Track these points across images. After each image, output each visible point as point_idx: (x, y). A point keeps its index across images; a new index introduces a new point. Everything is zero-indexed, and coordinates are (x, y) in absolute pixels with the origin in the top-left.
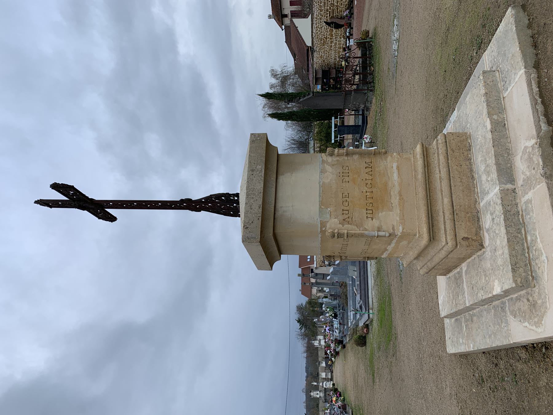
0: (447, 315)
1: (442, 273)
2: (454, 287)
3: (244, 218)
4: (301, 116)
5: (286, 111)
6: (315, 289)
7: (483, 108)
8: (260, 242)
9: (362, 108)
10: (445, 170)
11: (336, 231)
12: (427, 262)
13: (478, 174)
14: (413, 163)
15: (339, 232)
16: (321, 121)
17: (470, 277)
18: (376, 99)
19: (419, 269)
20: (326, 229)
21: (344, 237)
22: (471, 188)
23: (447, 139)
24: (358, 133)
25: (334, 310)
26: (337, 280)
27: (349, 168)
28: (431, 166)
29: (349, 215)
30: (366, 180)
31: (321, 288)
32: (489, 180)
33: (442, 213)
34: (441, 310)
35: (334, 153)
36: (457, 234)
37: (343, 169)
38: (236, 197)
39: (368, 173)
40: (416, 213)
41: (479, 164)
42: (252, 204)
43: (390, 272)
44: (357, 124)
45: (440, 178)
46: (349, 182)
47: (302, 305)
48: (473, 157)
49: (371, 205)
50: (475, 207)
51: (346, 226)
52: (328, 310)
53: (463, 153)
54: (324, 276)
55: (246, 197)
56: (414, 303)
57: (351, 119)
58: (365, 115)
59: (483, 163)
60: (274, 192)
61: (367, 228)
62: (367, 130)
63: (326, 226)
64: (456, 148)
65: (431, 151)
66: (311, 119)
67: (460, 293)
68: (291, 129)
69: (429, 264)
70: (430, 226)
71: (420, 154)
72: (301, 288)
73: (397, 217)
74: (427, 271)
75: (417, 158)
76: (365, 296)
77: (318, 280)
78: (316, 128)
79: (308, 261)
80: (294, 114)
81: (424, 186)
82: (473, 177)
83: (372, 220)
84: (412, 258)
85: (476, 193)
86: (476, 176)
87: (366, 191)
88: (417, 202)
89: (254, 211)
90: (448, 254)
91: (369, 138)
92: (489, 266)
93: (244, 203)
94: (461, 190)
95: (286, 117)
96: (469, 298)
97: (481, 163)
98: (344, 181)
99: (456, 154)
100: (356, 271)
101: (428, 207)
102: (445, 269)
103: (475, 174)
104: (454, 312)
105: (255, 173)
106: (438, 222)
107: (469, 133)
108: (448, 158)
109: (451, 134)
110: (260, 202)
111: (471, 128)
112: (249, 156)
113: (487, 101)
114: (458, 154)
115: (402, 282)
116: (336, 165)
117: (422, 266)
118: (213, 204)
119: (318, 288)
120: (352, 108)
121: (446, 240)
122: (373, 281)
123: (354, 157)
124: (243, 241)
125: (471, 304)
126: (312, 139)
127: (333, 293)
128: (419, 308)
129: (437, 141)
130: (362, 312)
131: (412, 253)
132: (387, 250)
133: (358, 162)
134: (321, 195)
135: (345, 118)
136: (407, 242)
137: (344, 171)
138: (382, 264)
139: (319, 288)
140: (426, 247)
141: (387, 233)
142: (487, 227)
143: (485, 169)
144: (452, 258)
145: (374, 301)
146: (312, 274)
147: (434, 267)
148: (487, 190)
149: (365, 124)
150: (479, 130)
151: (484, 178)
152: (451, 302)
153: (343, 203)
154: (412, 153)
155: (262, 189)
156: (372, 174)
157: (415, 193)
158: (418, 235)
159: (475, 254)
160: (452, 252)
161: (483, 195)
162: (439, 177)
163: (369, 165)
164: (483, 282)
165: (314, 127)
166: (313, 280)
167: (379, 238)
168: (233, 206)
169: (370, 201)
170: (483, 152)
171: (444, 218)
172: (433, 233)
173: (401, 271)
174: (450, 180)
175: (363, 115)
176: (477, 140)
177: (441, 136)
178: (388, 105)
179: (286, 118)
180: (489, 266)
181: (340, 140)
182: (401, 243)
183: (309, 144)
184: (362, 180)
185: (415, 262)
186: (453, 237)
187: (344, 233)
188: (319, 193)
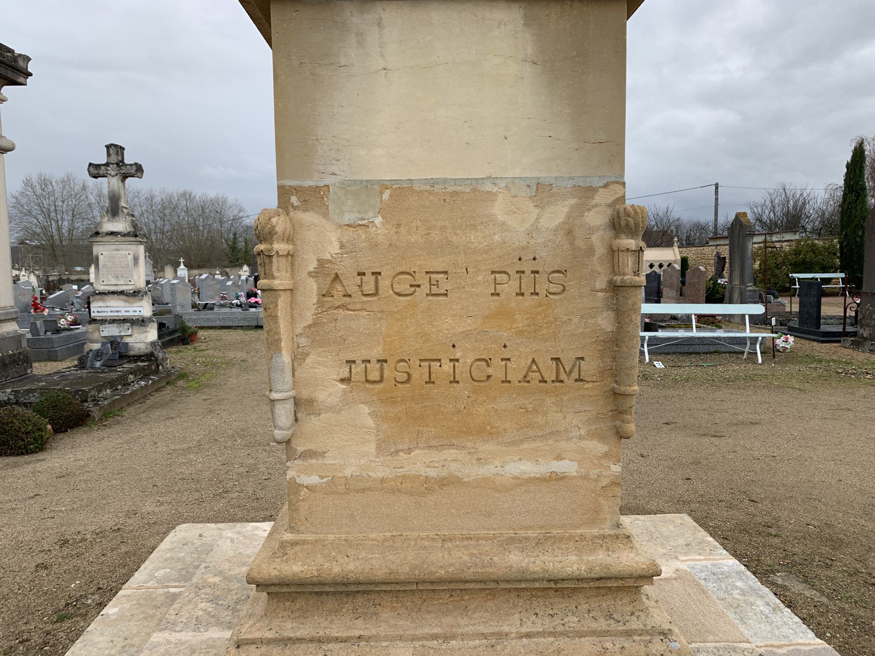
9: (862, 331)
11: (279, 247)
16: (839, 251)
20: (295, 208)
24: (801, 323)
27: (555, 297)
28: (557, 600)
29: (357, 297)
30: (502, 360)
33: (357, 633)
35: (623, 236)
37: (554, 272)
39: (534, 367)
44: (822, 321)
46: (520, 297)
58: (842, 339)
61: (308, 361)
62: (807, 342)
63: (307, 210)
66: (846, 232)
71: (607, 567)
73: (354, 468)
75: (592, 551)
80: (859, 196)
83: (342, 381)
87: (457, 360)
91: (786, 346)
95: (852, 179)
98: (497, 275)
101: (384, 583)
106: (330, 611)
120: (861, 312)
123: (605, 314)
133: (580, 331)
134: (437, 188)
137: (542, 278)
149: (822, 339)
156: (528, 382)
162: (506, 629)
163: (571, 372)
169: (419, 374)
175: (845, 334)
178: (862, 392)
183: (792, 233)
184: (505, 346)
188: (445, 181)
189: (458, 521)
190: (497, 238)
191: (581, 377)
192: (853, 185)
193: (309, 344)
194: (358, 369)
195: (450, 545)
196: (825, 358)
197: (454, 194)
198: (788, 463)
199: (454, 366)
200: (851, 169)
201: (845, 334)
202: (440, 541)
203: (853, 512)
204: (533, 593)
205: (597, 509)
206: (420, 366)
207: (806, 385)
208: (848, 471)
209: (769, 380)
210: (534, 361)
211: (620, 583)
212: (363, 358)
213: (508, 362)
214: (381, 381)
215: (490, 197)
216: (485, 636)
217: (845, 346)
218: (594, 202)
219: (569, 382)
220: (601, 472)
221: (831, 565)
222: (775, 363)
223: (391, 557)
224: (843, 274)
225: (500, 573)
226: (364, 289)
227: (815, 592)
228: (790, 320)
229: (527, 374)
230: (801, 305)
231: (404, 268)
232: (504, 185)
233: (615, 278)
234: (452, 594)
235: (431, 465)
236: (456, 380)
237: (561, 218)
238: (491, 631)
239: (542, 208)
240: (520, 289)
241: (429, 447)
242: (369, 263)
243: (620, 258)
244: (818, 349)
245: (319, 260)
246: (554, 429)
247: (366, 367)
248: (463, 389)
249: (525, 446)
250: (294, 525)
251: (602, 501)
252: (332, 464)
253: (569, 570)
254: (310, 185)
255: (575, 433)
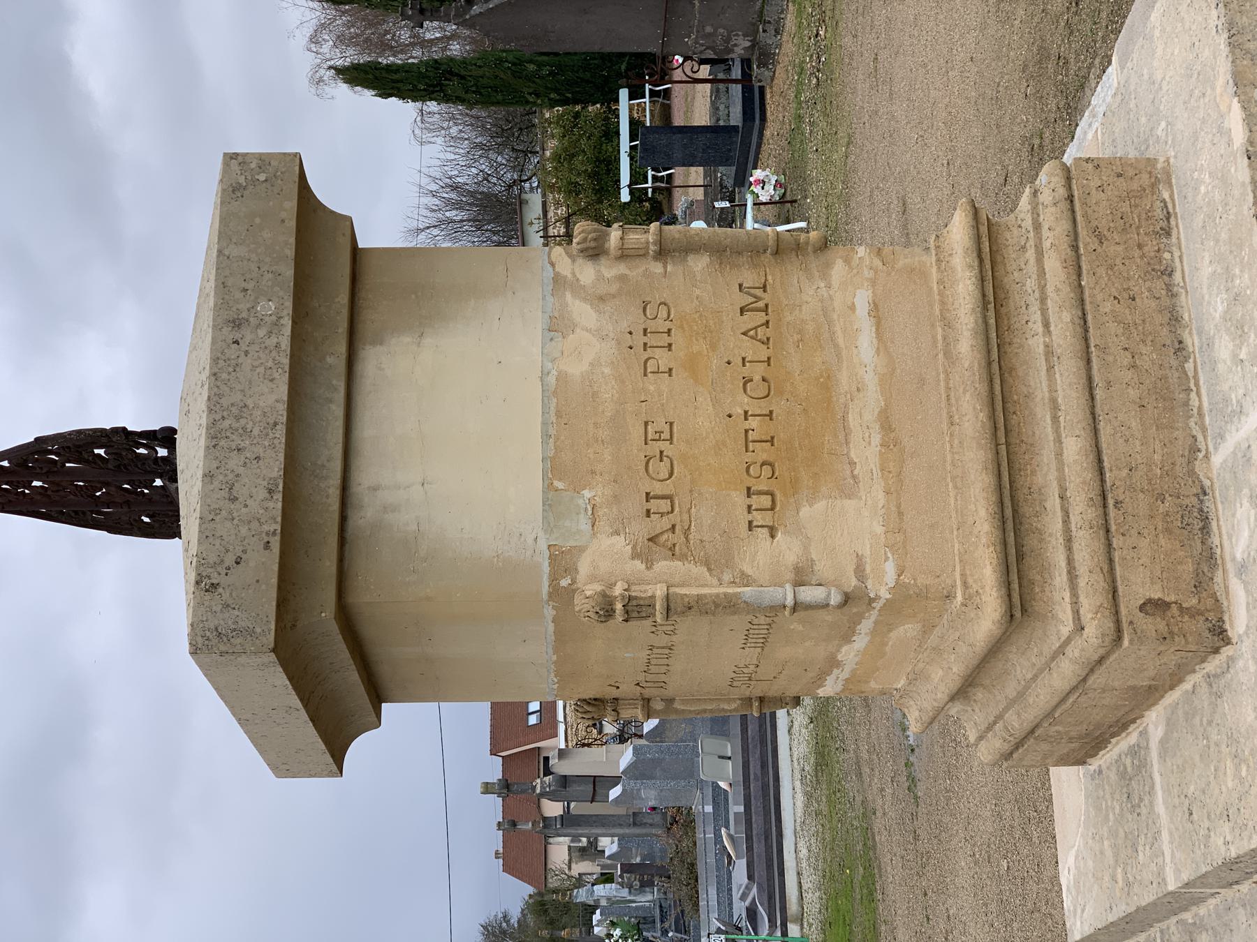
0: (1092, 930)
1: (1068, 754)
2: (1117, 811)
3: (200, 542)
4: (485, 81)
5: (416, 56)
6: (559, 844)
7: (1215, 58)
8: (274, 650)
9: (739, 51)
10: (1067, 317)
11: (618, 590)
12: (1006, 709)
13: (1200, 334)
14: (936, 292)
15: (633, 594)
16: (570, 107)
17: (1178, 766)
18: (800, 12)
19: (972, 739)
20: (574, 581)
21: (654, 616)
22: (1173, 393)
23: (1074, 187)
24: (726, 162)
25: (640, 932)
26: (652, 803)
30: (744, 365)
31: (588, 838)
32: (1241, 357)
33: (1058, 501)
34: (1069, 910)
35: (607, 245)
36: (1121, 589)
37: (645, 315)
38: (161, 446)
39: (752, 333)
40: (952, 502)
41: (1205, 291)
42: (238, 476)
43: (865, 756)
44: (721, 123)
45: (1049, 352)
47: (505, 917)
48: (1181, 262)
49: (767, 471)
50: (1192, 473)
51: (663, 566)
52: (617, 932)
53: (1140, 246)
54: (597, 785)
55: (207, 448)
56: (966, 886)
57: (699, 96)
58: (757, 85)
59: (1218, 288)
60: (340, 423)
62: (764, 148)
64: (1112, 225)
65: (1011, 238)
66: (530, 94)
67: (1143, 837)
68: (440, 140)
69: (1011, 716)
70: (1009, 558)
71: (966, 251)
72: (501, 844)
74: (1007, 747)
76: (769, 866)
77: (573, 805)
78: (553, 136)
79: (530, 723)
80: (451, 73)
81: (982, 388)
82: (1180, 348)
83: (773, 537)
84: (942, 695)
85: (1195, 410)
86: (1193, 341)
87: (746, 412)
88: (957, 457)
89: (244, 510)
90: (1084, 674)
92: (1249, 719)
93: (200, 473)
94: (1134, 402)
96: (1178, 855)
97: (1210, 286)
98: (649, 370)
99: (1112, 248)
100: (730, 758)
101: (999, 476)
102: (1080, 737)
103: (1190, 333)
104: (1120, 919)
105: (247, 335)
106: (1041, 541)
107: (1162, 159)
108: (1080, 267)
109: (1090, 166)
110: (274, 466)
111: (1170, 138)
112: (218, 256)
113: (1231, 25)
114: (1120, 248)
115: (916, 798)
116: (614, 296)
117: (983, 727)
118: (51, 479)
119: (576, 838)
120: (701, 52)
121: (1076, 614)
122: (800, 799)
124: (195, 651)
125: (1186, 881)
126: (535, 184)
127: (638, 860)
128: (986, 905)
129: (1035, 193)
130: (756, 934)
131: (941, 673)
132: (838, 664)
134: (552, 431)
135: (674, 94)
136: (919, 626)
137: (652, 326)
138: (835, 724)
139: (580, 841)
140: (996, 649)
141: (833, 590)
142: (1239, 556)
143: (1226, 312)
144: (1104, 691)
145: (805, 887)
146: (547, 779)
147: (1032, 731)
148: (1238, 402)
149: (757, 122)
150: (1201, 149)
151: (1224, 349)
152: (1106, 878)
153: (647, 463)
154: (932, 245)
155: (282, 408)
157: (945, 415)
158: (959, 598)
159: (1194, 671)
160: (1101, 661)
161: (1223, 423)
162: (1042, 347)
164: (1230, 784)
165: (543, 133)
166: (553, 809)
167: (801, 614)
168: (150, 487)
169: (762, 452)
170: (1217, 241)
171: (1066, 521)
172: (1020, 586)
173: (913, 750)
174: (1089, 361)
175: (746, 79)
176: (1196, 189)
177: (1051, 175)
178: (847, 41)
179: (415, 88)
180: (1249, 719)
181: (655, 190)
182: (893, 635)
183: (525, 208)
185: (954, 709)
186: (1102, 599)
187: (653, 597)
188: (544, 424)
189: (931, 412)
190: (607, 371)
191: (762, 286)
192: (426, 84)
193: (730, 571)
194: (759, 518)
195: (956, 417)
196: (793, 111)
197: (559, 414)
198: (955, 140)
199: (752, 415)
200: (392, 88)
201: (746, 79)
202: (953, 427)
203: (1007, 37)
204: (1006, 328)
205: (909, 269)
206: (754, 451)
207: (840, 134)
208: (959, 50)
209: (835, 200)
210: (745, 334)
211: (985, 240)
212: (746, 512)
213: (747, 360)
214: (772, 495)
215: (562, 377)
216: (1050, 368)
217: (769, 81)
218: (569, 276)
219: (767, 298)
220: (866, 266)
221: (1065, 58)
222: (806, 197)
223: (972, 477)
224: (621, 91)
225: (979, 356)
226: (665, 511)
227: (1091, 74)
228: (721, 185)
229: (759, 341)
230: (689, 162)
231: (642, 468)
232: (550, 364)
233: (651, 252)
234: (1012, 411)
235: (867, 440)
236: (768, 413)
237: (587, 308)
238: (1044, 363)
239: (575, 325)
240: (664, 347)
241: (847, 443)
242: (636, 504)
243: (630, 247)
244: (777, 125)
245: (633, 558)
246: (821, 313)
247: (757, 510)
248: (778, 406)
249: (841, 341)
250: (945, 591)
251: (900, 264)
252: (871, 547)
253: (971, 288)
254: (547, 565)
255: (823, 292)
